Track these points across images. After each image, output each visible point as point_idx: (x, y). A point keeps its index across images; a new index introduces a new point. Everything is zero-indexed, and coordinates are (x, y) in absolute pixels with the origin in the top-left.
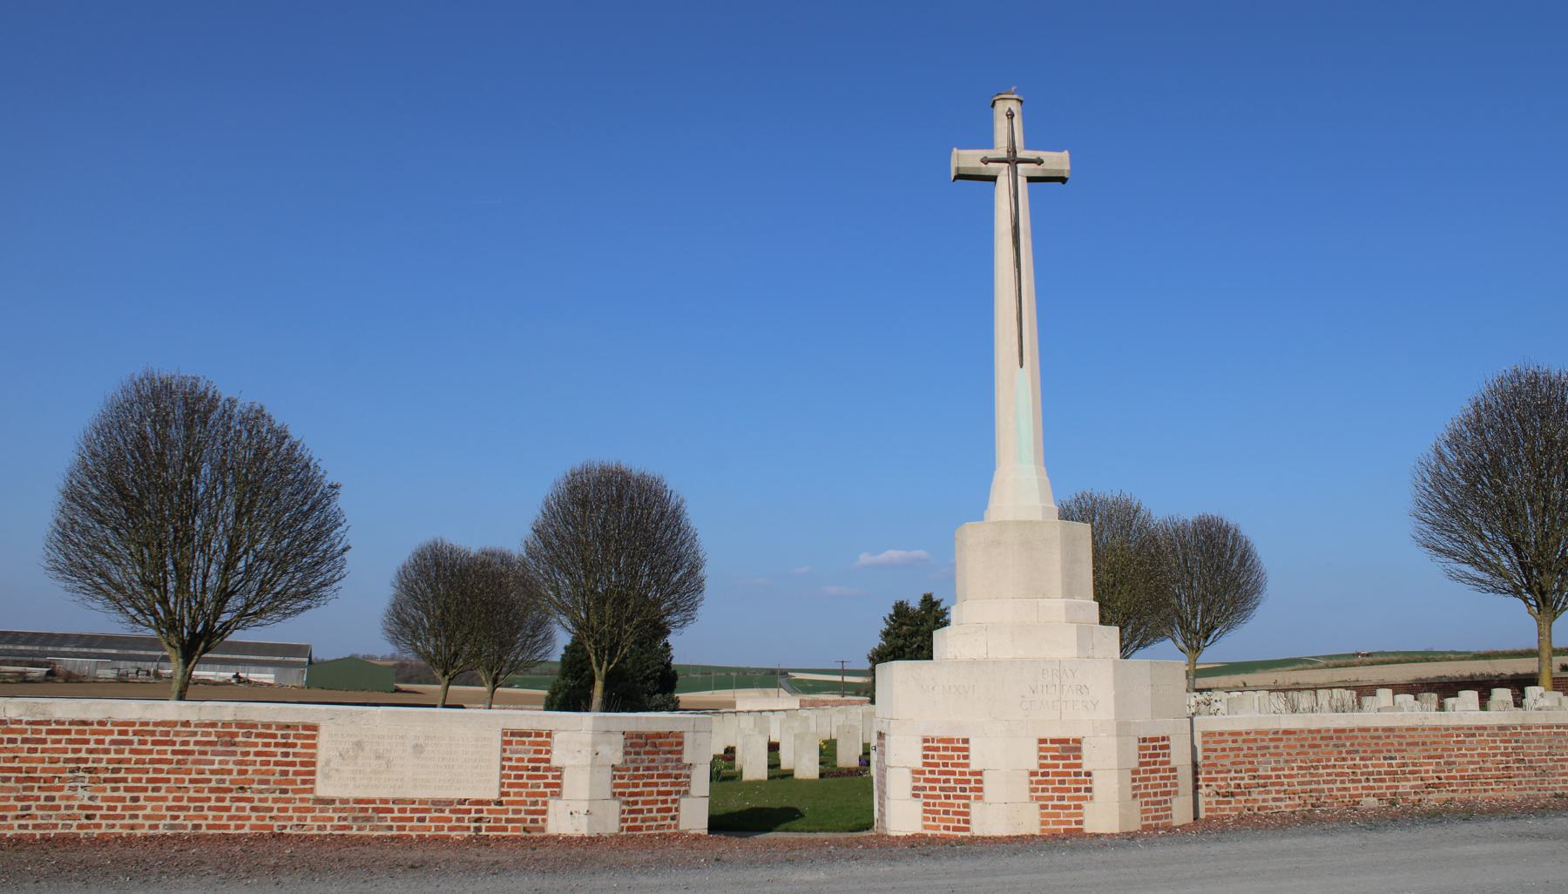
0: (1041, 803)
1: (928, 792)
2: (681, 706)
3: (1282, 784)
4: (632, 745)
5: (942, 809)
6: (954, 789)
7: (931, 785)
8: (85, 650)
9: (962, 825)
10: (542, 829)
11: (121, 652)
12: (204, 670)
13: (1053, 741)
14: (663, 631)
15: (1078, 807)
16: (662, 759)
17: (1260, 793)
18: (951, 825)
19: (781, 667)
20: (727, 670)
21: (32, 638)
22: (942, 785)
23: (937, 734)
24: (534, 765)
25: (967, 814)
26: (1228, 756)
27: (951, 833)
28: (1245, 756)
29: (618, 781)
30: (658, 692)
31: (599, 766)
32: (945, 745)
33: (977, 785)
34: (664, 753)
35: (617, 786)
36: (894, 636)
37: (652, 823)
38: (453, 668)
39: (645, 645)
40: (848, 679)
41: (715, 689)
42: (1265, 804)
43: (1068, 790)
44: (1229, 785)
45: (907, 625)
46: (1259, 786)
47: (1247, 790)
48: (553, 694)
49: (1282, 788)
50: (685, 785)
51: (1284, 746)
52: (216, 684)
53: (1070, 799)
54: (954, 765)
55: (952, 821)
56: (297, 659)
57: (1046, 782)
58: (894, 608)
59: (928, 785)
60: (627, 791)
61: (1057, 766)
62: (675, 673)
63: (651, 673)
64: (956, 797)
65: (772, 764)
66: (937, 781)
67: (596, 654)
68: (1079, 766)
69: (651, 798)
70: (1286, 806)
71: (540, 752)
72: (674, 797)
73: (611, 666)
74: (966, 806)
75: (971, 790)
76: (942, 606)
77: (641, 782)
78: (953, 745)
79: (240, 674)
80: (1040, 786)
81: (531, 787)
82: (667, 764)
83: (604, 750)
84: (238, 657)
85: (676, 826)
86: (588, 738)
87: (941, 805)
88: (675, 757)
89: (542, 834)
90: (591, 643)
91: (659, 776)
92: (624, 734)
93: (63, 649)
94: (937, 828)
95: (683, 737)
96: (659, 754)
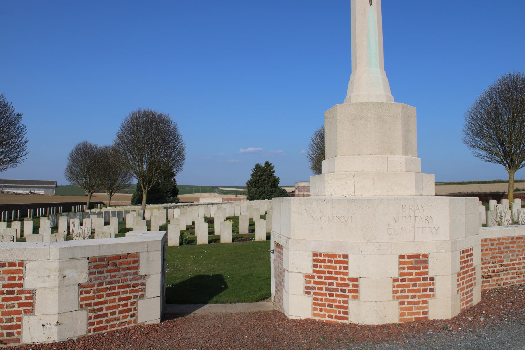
0: (400, 300)
1: (317, 291)
2: (180, 201)
3: (515, 269)
4: (95, 267)
5: (327, 303)
6: (337, 290)
7: (319, 286)
9: (342, 315)
10: (18, 340)
13: (409, 257)
14: (173, 175)
15: (425, 302)
16: (122, 274)
17: (504, 275)
18: (334, 315)
19: (216, 186)
20: (198, 187)
22: (327, 286)
23: (324, 250)
24: (8, 289)
25: (346, 308)
26: (488, 254)
27: (334, 320)
28: (497, 253)
29: (84, 295)
30: (172, 196)
31: (67, 286)
32: (330, 259)
33: (354, 288)
34: (124, 269)
35: (83, 299)
36: (255, 176)
37: (115, 323)
38: (92, 189)
39: (167, 179)
40: (238, 189)
41: (194, 193)
42: (507, 281)
43: (419, 291)
44: (489, 271)
45: (260, 172)
46: (504, 271)
47: (498, 273)
48: (134, 197)
49: (515, 271)
50: (142, 291)
51: (517, 246)
52: (23, 195)
53: (420, 297)
54: (336, 273)
55: (335, 312)
56: (51, 186)
57: (405, 286)
58: (255, 166)
59: (317, 286)
60: (93, 302)
61: (411, 274)
62: (178, 189)
63: (169, 190)
64: (338, 296)
65: (211, 231)
66: (324, 283)
67: (143, 184)
68: (426, 273)
69: (114, 304)
70: (517, 282)
71: (14, 278)
72: (132, 300)
73: (149, 189)
74: (345, 302)
75: (350, 291)
76: (272, 166)
77: (105, 294)
78: (336, 259)
79: (32, 191)
80: (400, 289)
81: (7, 308)
82: (126, 278)
83: (70, 273)
84: (31, 185)
85: (135, 321)
86: (55, 265)
87: (326, 300)
88: (132, 271)
89: (17, 344)
90: (141, 180)
91: (120, 287)
92: (88, 258)
94: (324, 316)
95: (138, 257)
96: (119, 271)
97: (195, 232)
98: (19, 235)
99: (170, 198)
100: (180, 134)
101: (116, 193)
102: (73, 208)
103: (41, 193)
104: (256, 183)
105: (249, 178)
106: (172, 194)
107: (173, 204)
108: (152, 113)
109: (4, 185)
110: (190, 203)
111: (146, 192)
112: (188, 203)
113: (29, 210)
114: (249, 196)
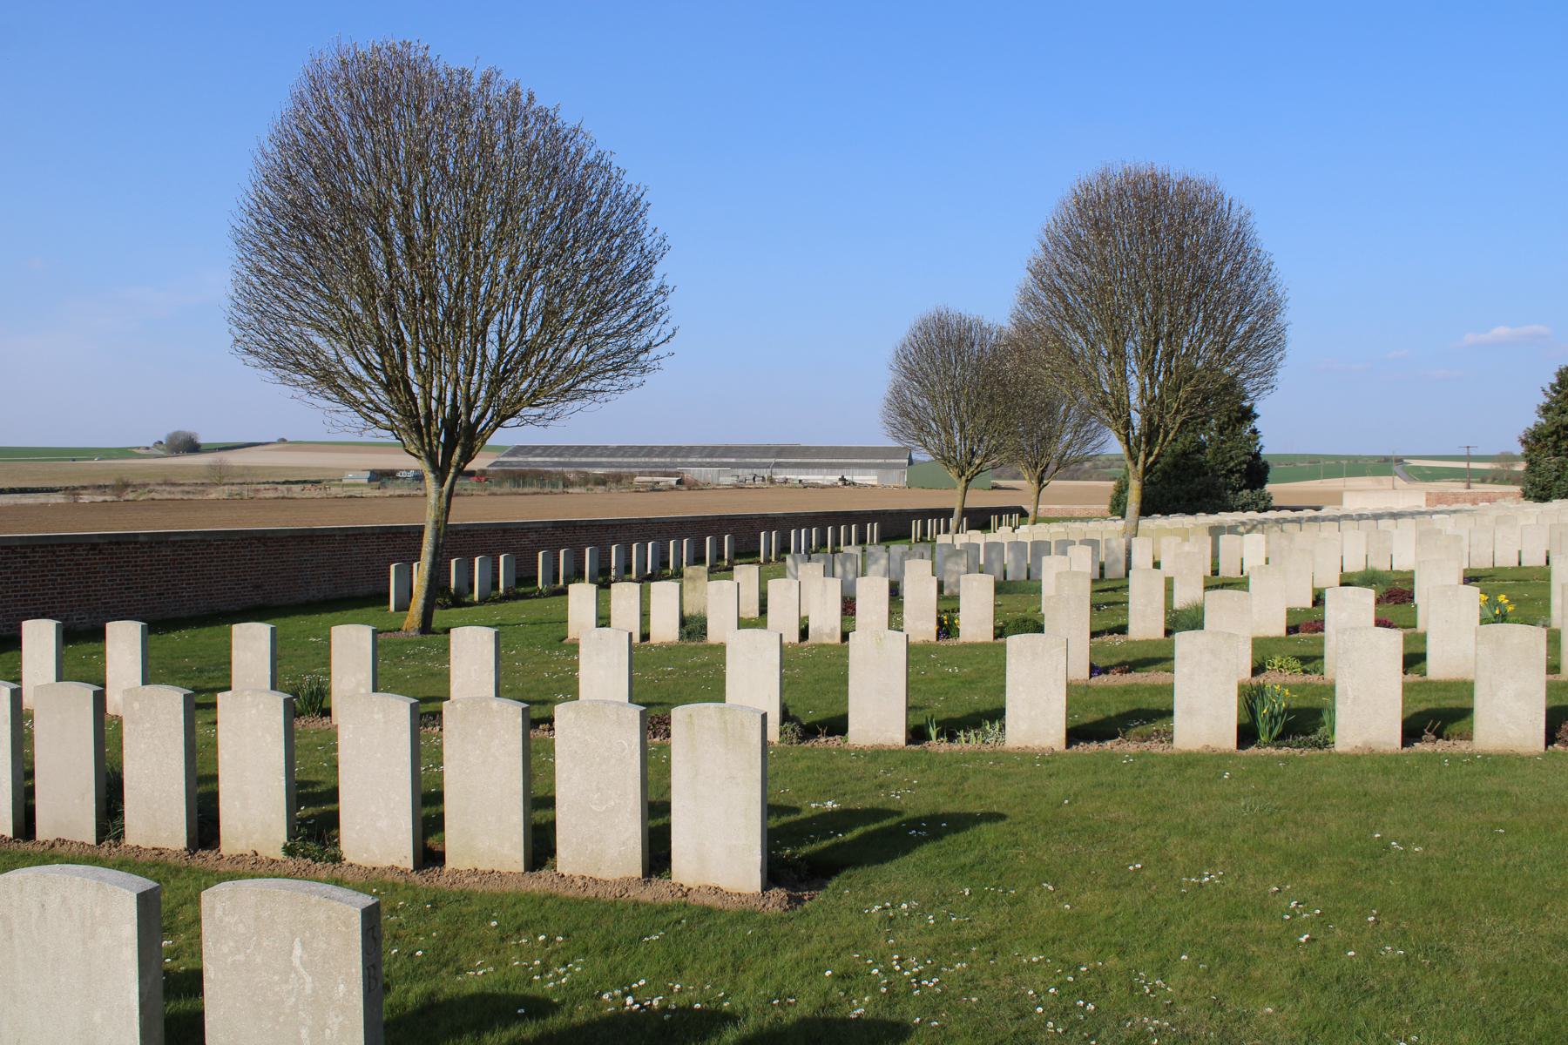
2: (1274, 503)
8: (708, 460)
11: (739, 460)
12: (813, 474)
21: (664, 451)
30: (1245, 487)
36: (1557, 411)
39: (1227, 432)
40: (1474, 465)
52: (823, 487)
58: (1557, 375)
63: (1236, 465)
84: (842, 461)
93: (690, 460)
97: (1326, 655)
98: (752, 611)
99: (1240, 493)
100: (1263, 249)
101: (1055, 479)
102: (916, 527)
103: (871, 483)
104: (1558, 436)
105: (1530, 419)
106: (1244, 482)
107: (1249, 513)
108: (1153, 175)
109: (778, 460)
110: (1309, 512)
111: (1140, 473)
112: (1301, 510)
113: (793, 531)
114: (1533, 484)
